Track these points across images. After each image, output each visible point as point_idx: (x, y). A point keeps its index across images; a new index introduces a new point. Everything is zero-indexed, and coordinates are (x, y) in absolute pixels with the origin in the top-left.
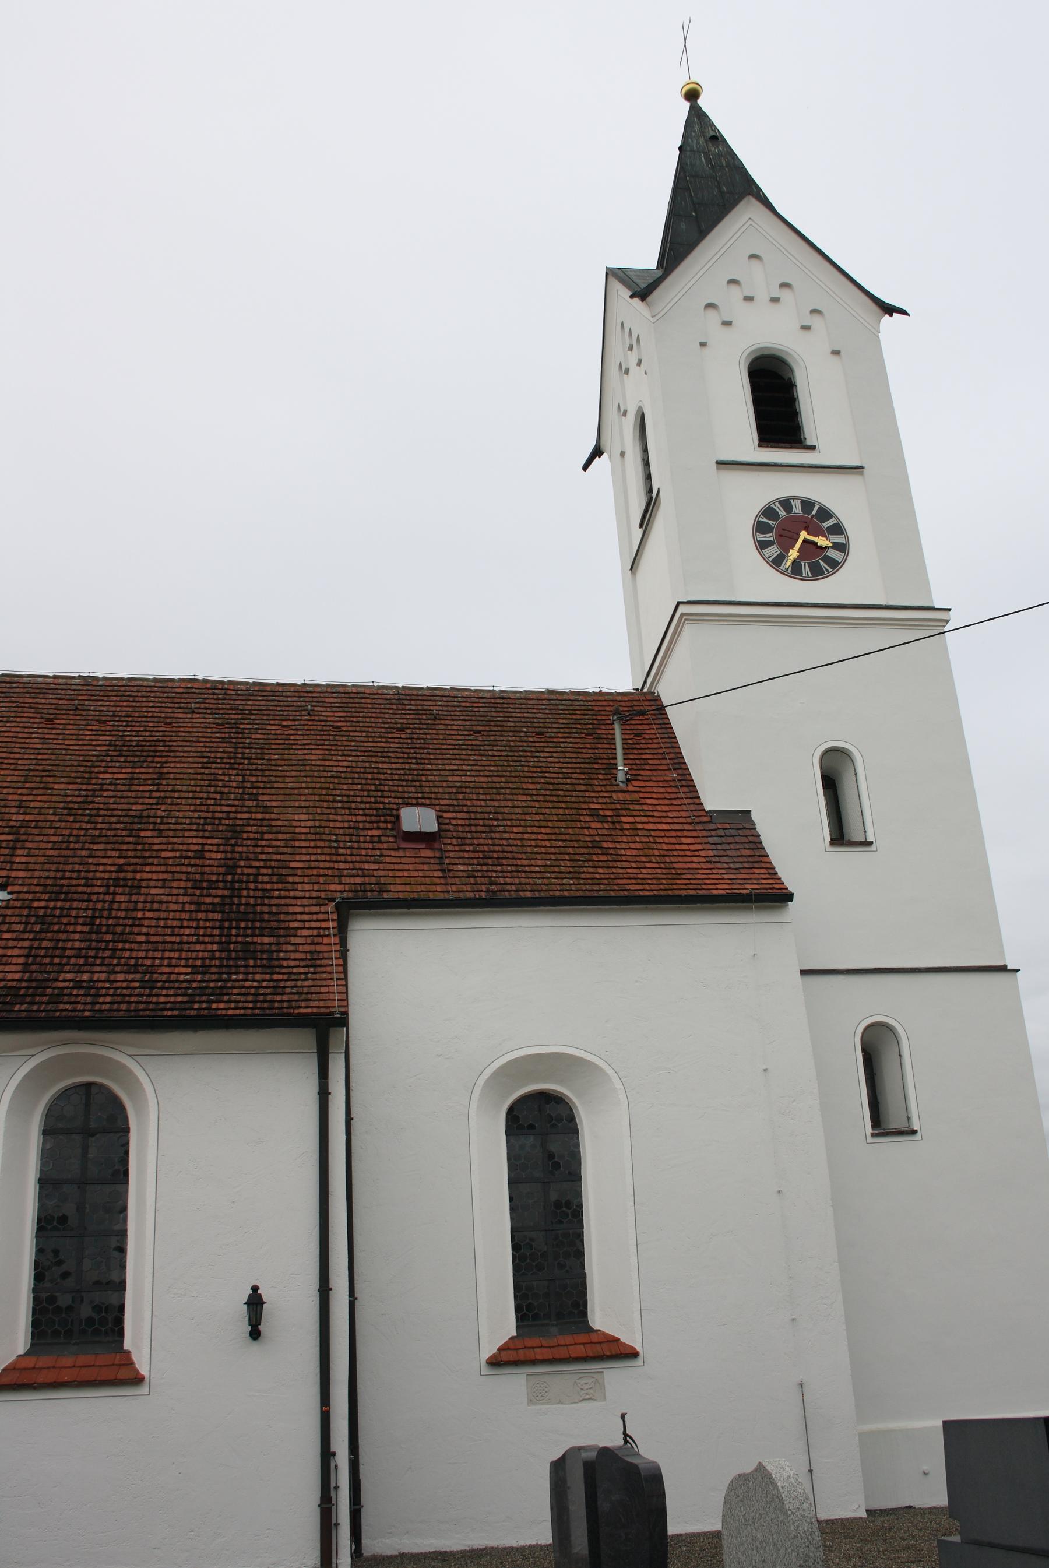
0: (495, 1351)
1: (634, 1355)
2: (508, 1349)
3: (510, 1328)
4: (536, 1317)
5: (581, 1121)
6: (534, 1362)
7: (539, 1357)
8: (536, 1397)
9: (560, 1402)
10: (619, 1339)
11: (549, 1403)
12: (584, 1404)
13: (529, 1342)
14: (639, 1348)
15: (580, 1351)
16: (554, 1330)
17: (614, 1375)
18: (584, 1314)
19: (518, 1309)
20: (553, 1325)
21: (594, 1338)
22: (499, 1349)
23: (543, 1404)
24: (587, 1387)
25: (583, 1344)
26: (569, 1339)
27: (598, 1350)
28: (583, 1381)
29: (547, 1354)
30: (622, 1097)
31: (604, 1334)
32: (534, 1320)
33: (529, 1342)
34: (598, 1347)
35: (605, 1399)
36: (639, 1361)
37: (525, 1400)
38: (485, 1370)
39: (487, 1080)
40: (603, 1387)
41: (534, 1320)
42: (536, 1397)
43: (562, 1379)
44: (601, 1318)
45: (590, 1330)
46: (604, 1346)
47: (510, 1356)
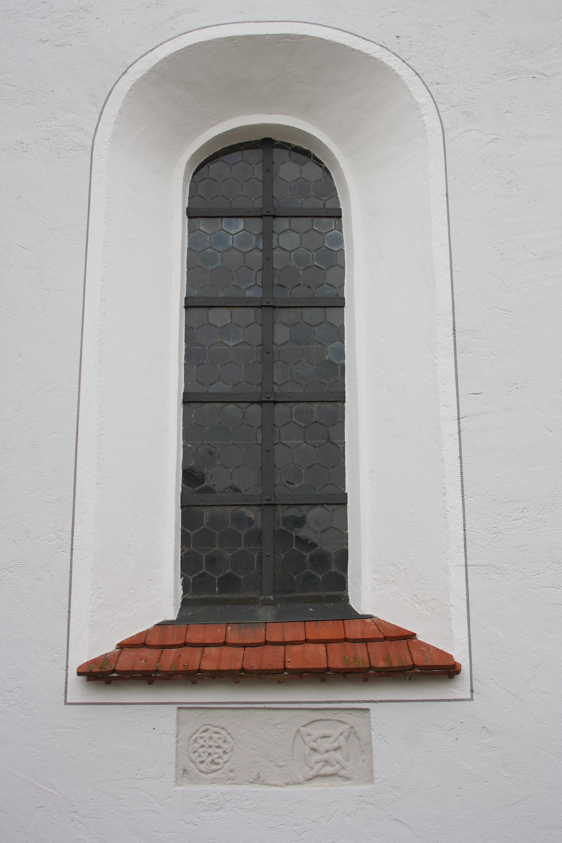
0: (110, 647)
1: (445, 670)
2: (145, 645)
3: (158, 597)
4: (229, 582)
5: (346, 192)
6: (194, 677)
7: (207, 665)
8: (199, 764)
9: (258, 780)
10: (412, 636)
11: (230, 780)
12: (317, 787)
13: (197, 634)
14: (460, 656)
15: (315, 657)
16: (265, 613)
17: (394, 718)
18: (340, 582)
19: (188, 563)
20: (267, 603)
21: (354, 630)
22: (122, 646)
23: (214, 781)
24: (326, 745)
25: (326, 642)
26: (294, 631)
27: (359, 656)
28: (317, 730)
29: (232, 659)
30: (431, 120)
31: (380, 624)
32: (223, 590)
33: (197, 634)
34: (360, 650)
35: (371, 779)
36: (459, 688)
37: (171, 770)
38: (78, 689)
39: (136, 85)
40: (366, 747)
41: (223, 590)
42: (199, 764)
43: (268, 722)
44: (372, 592)
45: (354, 616)
46: (375, 648)
47: (144, 660)
